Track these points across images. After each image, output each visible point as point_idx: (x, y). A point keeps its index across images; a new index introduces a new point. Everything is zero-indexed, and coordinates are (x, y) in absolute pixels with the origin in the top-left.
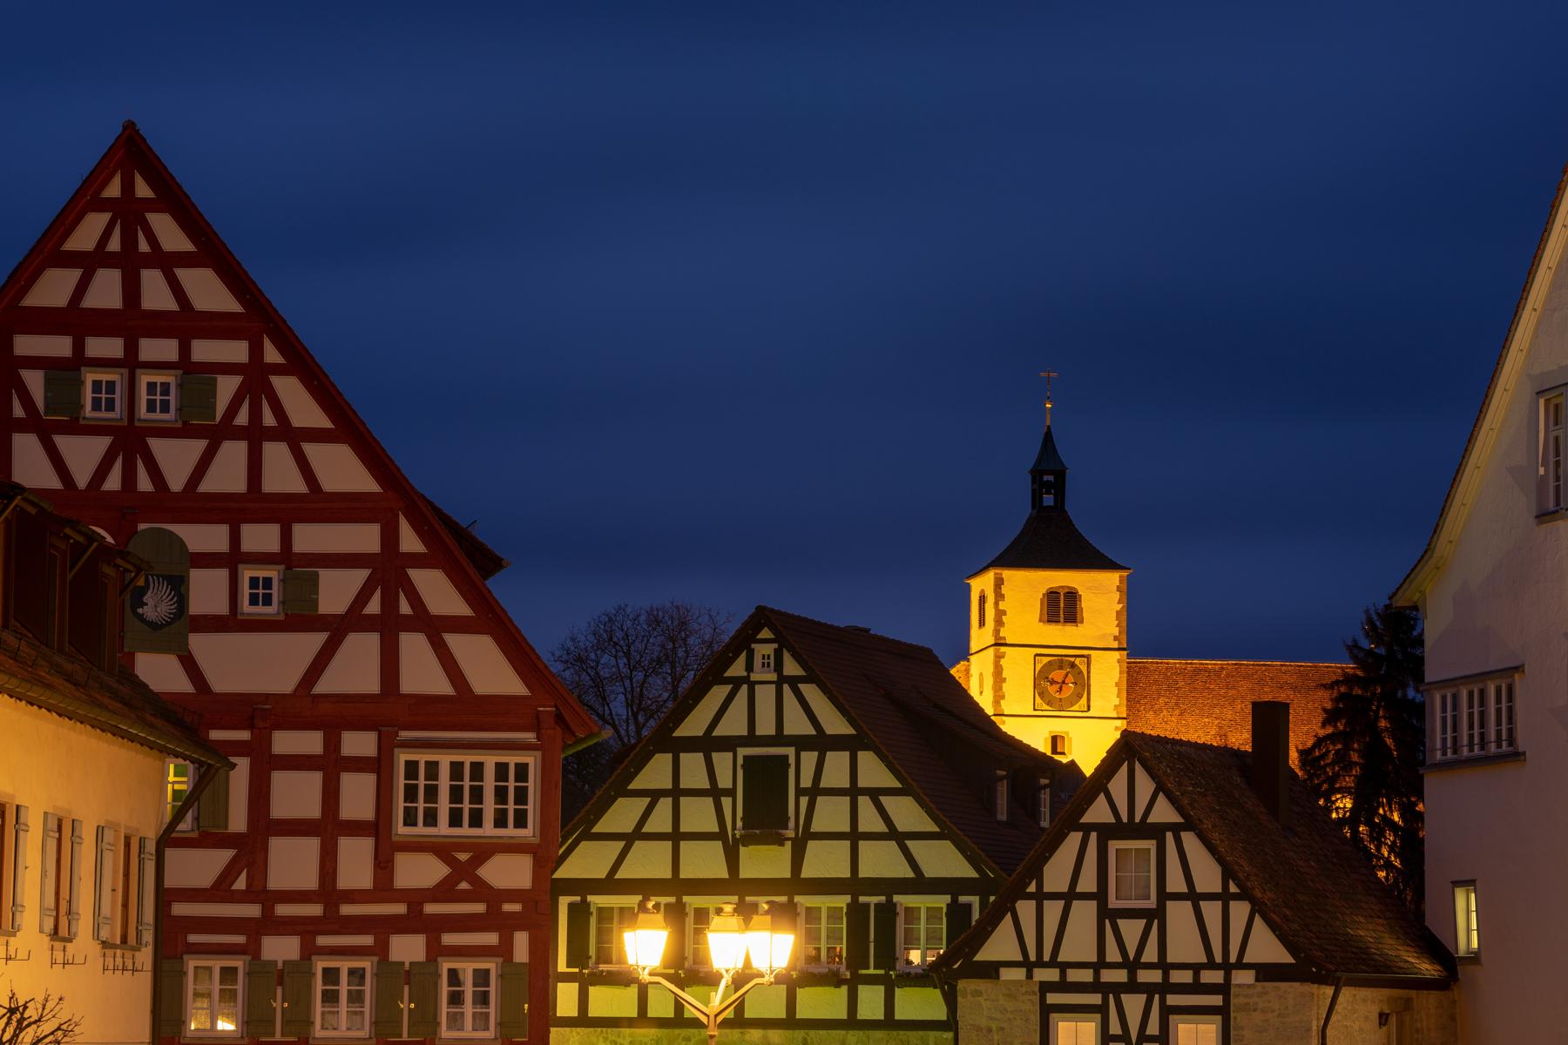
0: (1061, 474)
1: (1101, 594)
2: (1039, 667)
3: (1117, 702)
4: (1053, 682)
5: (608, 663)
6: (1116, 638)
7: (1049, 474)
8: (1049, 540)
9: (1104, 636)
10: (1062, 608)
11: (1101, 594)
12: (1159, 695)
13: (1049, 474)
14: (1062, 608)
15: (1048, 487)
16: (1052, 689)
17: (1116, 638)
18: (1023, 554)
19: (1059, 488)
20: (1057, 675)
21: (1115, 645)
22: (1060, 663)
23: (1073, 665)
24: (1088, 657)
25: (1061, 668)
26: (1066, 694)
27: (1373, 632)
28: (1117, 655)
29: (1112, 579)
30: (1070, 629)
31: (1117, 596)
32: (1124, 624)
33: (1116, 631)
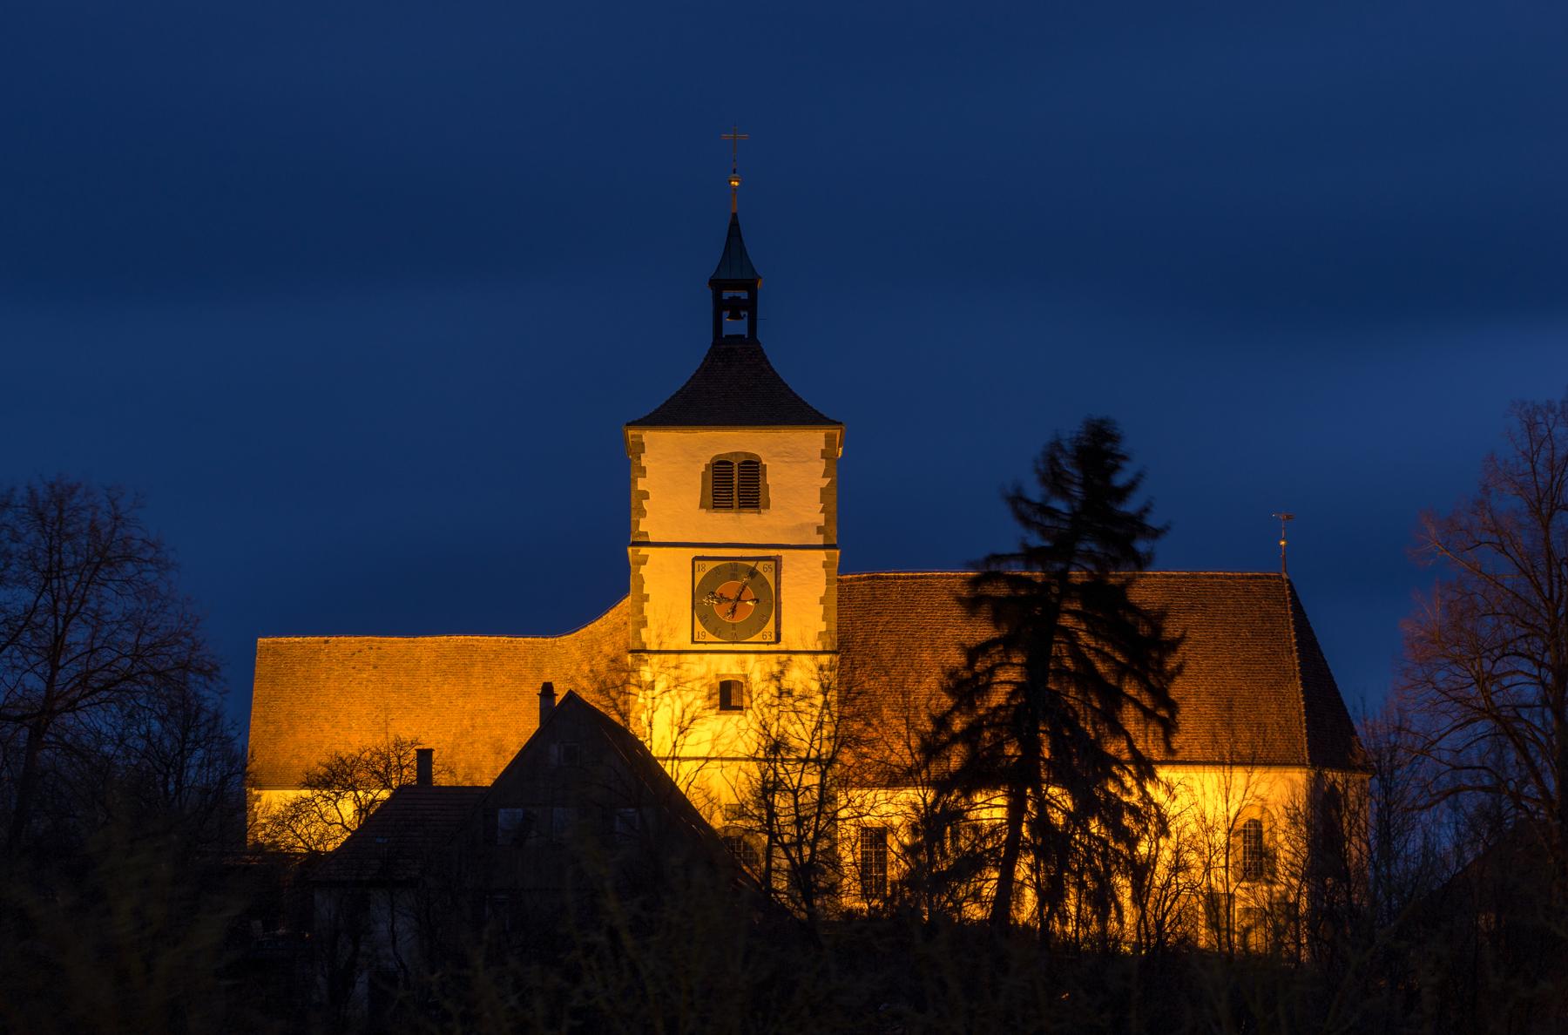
0: (751, 285)
1: (797, 465)
2: (699, 576)
3: (823, 627)
4: (722, 599)
5: (271, 728)
6: (820, 530)
7: (735, 289)
8: (732, 386)
9: (801, 528)
10: (735, 485)
11: (797, 465)
12: (946, 625)
13: (735, 289)
14: (735, 485)
15: (735, 308)
16: (721, 611)
17: (820, 530)
18: (682, 411)
19: (750, 307)
20: (729, 588)
21: (820, 540)
22: (732, 569)
23: (753, 573)
24: (777, 561)
25: (734, 577)
26: (740, 619)
27: (1054, 479)
28: (822, 555)
29: (813, 440)
30: (749, 518)
31: (821, 466)
32: (833, 508)
33: (820, 519)
